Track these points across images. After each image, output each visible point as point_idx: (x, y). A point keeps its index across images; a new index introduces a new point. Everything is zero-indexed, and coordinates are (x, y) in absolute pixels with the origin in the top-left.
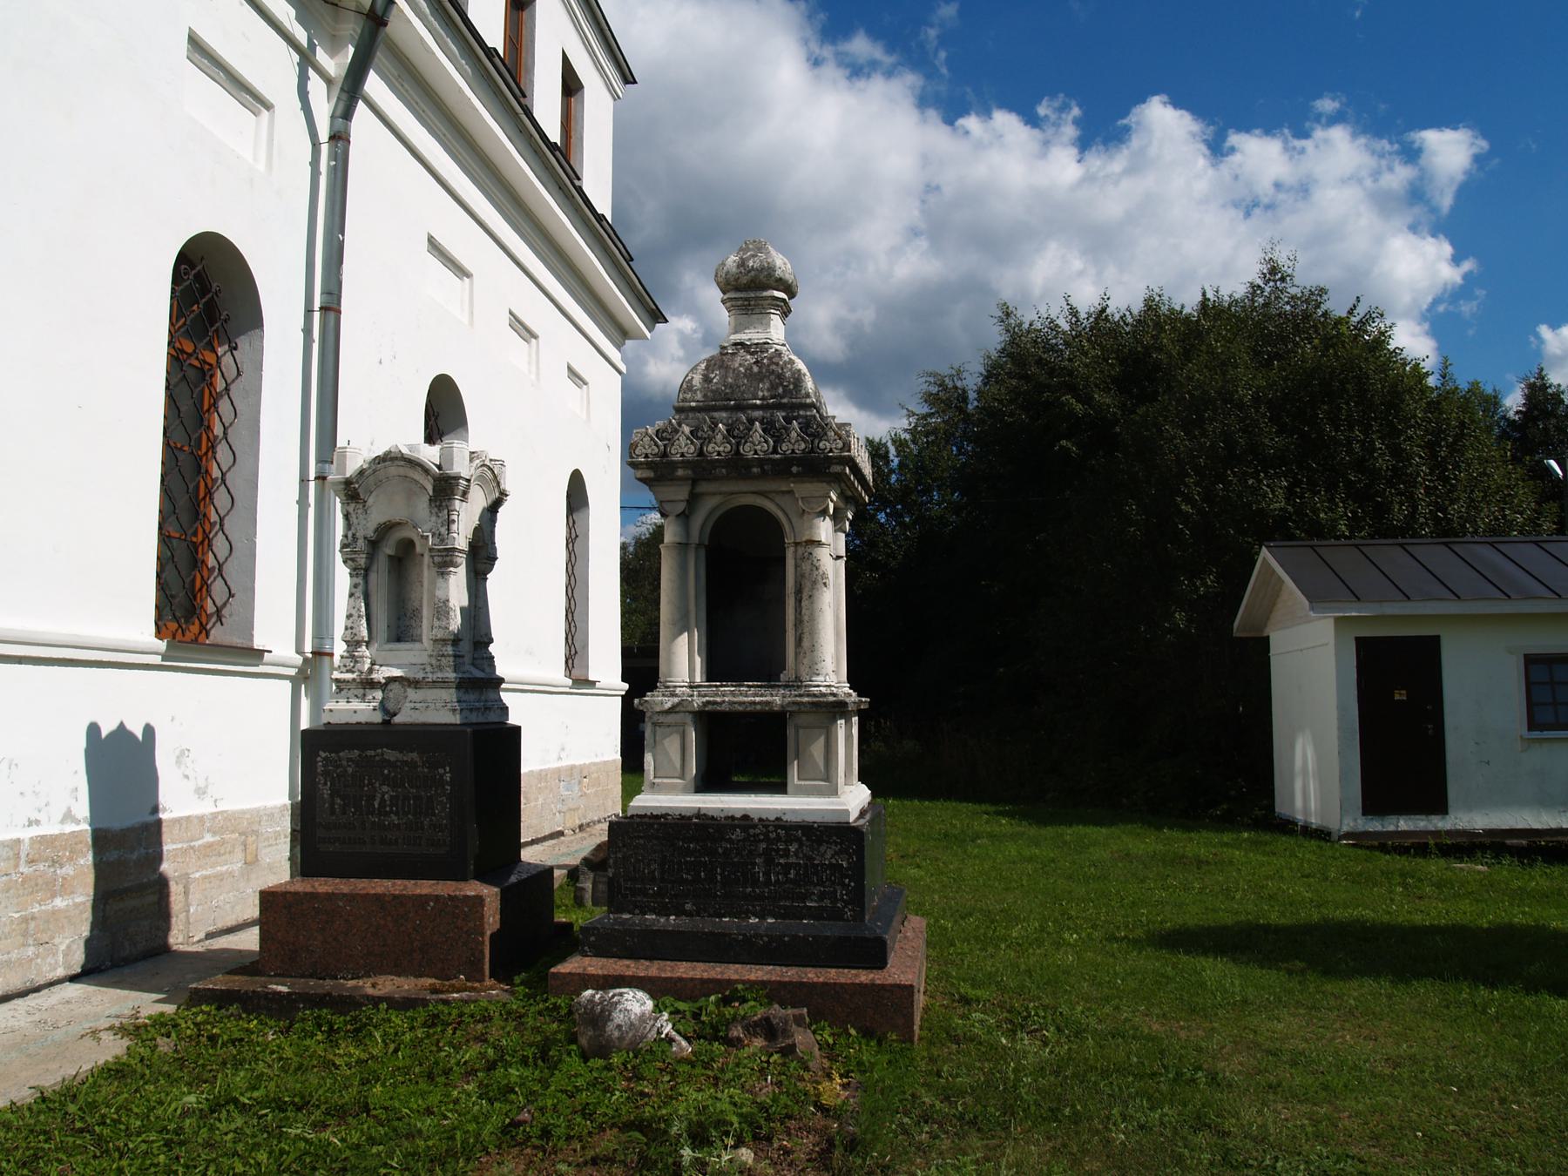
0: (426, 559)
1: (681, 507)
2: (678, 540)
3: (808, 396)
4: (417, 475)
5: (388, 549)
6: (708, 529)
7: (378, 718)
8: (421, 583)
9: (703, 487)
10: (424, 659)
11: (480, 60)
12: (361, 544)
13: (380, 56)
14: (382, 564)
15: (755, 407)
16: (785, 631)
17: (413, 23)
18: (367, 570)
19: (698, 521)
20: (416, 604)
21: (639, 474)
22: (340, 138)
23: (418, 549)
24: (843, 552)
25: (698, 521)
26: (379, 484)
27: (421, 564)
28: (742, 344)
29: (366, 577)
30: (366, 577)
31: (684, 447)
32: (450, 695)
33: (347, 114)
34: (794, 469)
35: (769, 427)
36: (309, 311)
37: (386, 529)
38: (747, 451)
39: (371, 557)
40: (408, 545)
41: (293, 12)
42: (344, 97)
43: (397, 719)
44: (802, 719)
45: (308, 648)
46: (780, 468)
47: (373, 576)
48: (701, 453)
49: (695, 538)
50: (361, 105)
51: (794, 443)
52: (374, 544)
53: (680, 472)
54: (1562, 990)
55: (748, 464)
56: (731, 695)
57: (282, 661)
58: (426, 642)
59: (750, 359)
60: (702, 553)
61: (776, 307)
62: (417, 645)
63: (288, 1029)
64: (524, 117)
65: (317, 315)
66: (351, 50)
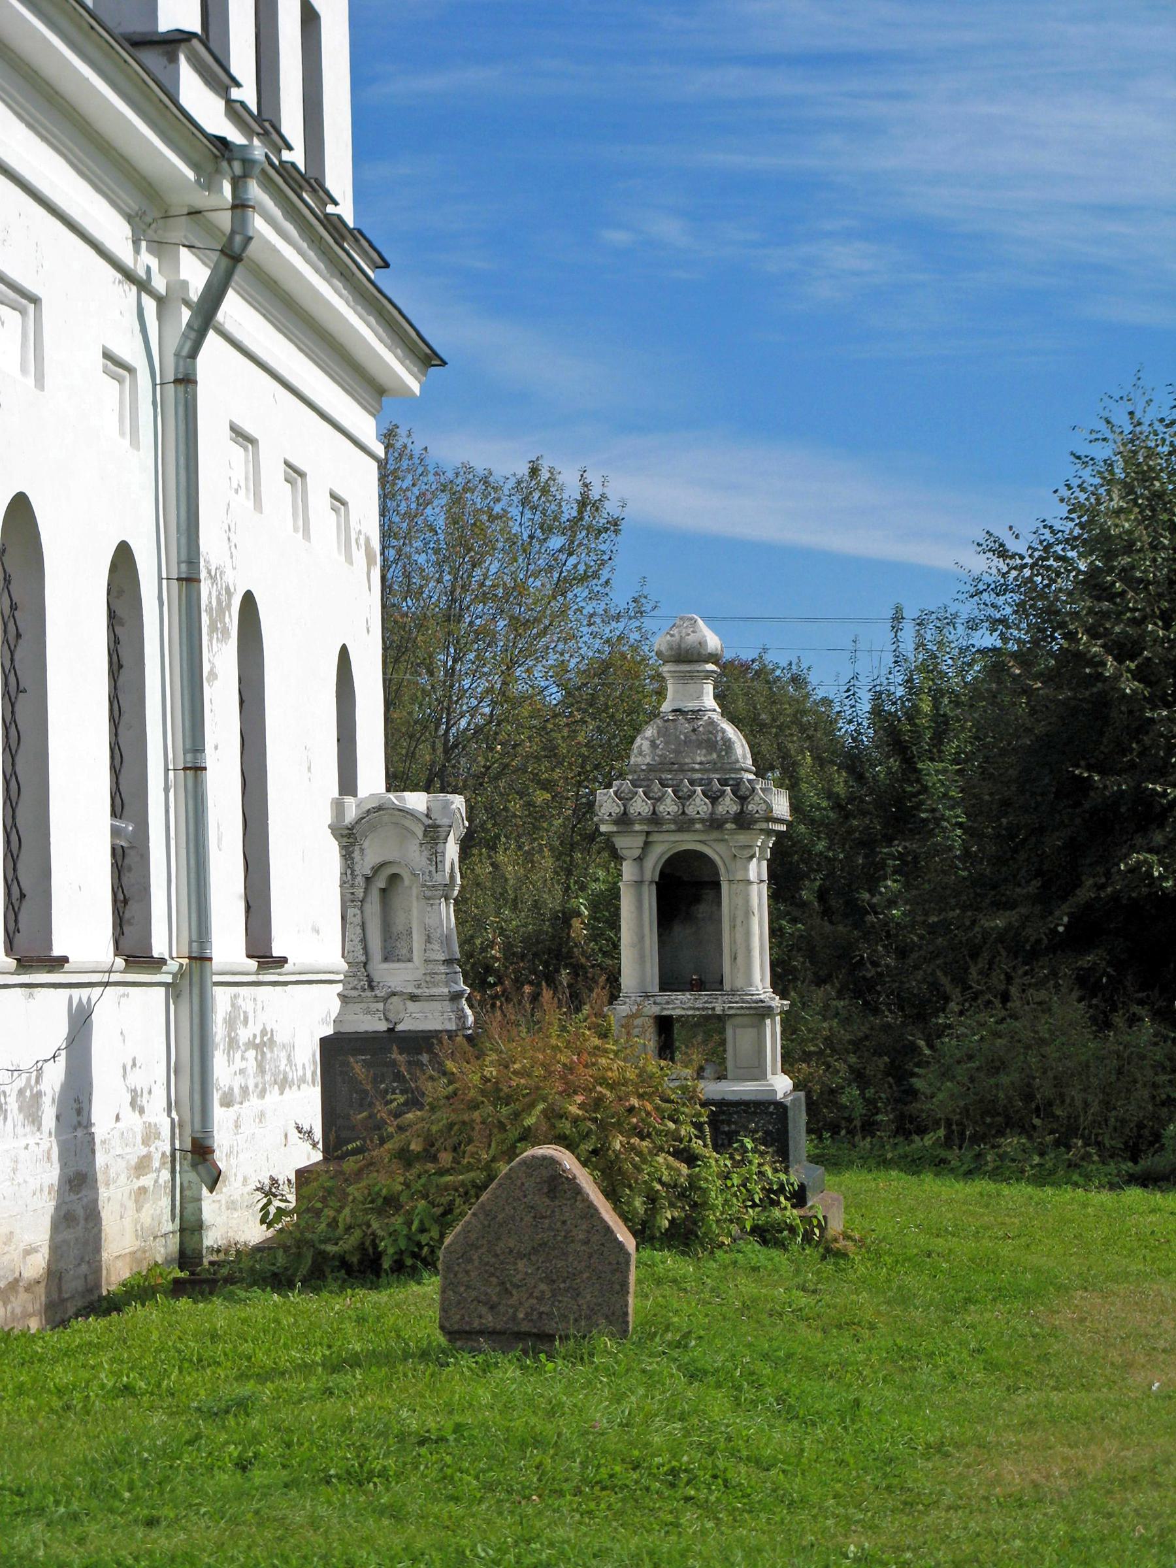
0: (415, 891)
1: (637, 853)
2: (635, 878)
3: (738, 761)
4: (408, 823)
5: (381, 883)
7: (383, 1026)
11: (281, 191)
12: (360, 880)
14: (375, 895)
15: (694, 770)
16: (137, 129)
20: (400, 928)
23: (407, 882)
24: (765, 877)
26: (373, 828)
34: (729, 826)
37: (377, 869)
38: (691, 811)
41: (125, 229)
43: (399, 1028)
44: (738, 1020)
46: (715, 824)
47: (368, 907)
48: (654, 813)
49: (648, 876)
50: (211, 334)
53: (637, 827)
54: (1138, 1158)
55: (692, 821)
56: (681, 1004)
57: (227, 968)
59: (687, 727)
62: (409, 965)
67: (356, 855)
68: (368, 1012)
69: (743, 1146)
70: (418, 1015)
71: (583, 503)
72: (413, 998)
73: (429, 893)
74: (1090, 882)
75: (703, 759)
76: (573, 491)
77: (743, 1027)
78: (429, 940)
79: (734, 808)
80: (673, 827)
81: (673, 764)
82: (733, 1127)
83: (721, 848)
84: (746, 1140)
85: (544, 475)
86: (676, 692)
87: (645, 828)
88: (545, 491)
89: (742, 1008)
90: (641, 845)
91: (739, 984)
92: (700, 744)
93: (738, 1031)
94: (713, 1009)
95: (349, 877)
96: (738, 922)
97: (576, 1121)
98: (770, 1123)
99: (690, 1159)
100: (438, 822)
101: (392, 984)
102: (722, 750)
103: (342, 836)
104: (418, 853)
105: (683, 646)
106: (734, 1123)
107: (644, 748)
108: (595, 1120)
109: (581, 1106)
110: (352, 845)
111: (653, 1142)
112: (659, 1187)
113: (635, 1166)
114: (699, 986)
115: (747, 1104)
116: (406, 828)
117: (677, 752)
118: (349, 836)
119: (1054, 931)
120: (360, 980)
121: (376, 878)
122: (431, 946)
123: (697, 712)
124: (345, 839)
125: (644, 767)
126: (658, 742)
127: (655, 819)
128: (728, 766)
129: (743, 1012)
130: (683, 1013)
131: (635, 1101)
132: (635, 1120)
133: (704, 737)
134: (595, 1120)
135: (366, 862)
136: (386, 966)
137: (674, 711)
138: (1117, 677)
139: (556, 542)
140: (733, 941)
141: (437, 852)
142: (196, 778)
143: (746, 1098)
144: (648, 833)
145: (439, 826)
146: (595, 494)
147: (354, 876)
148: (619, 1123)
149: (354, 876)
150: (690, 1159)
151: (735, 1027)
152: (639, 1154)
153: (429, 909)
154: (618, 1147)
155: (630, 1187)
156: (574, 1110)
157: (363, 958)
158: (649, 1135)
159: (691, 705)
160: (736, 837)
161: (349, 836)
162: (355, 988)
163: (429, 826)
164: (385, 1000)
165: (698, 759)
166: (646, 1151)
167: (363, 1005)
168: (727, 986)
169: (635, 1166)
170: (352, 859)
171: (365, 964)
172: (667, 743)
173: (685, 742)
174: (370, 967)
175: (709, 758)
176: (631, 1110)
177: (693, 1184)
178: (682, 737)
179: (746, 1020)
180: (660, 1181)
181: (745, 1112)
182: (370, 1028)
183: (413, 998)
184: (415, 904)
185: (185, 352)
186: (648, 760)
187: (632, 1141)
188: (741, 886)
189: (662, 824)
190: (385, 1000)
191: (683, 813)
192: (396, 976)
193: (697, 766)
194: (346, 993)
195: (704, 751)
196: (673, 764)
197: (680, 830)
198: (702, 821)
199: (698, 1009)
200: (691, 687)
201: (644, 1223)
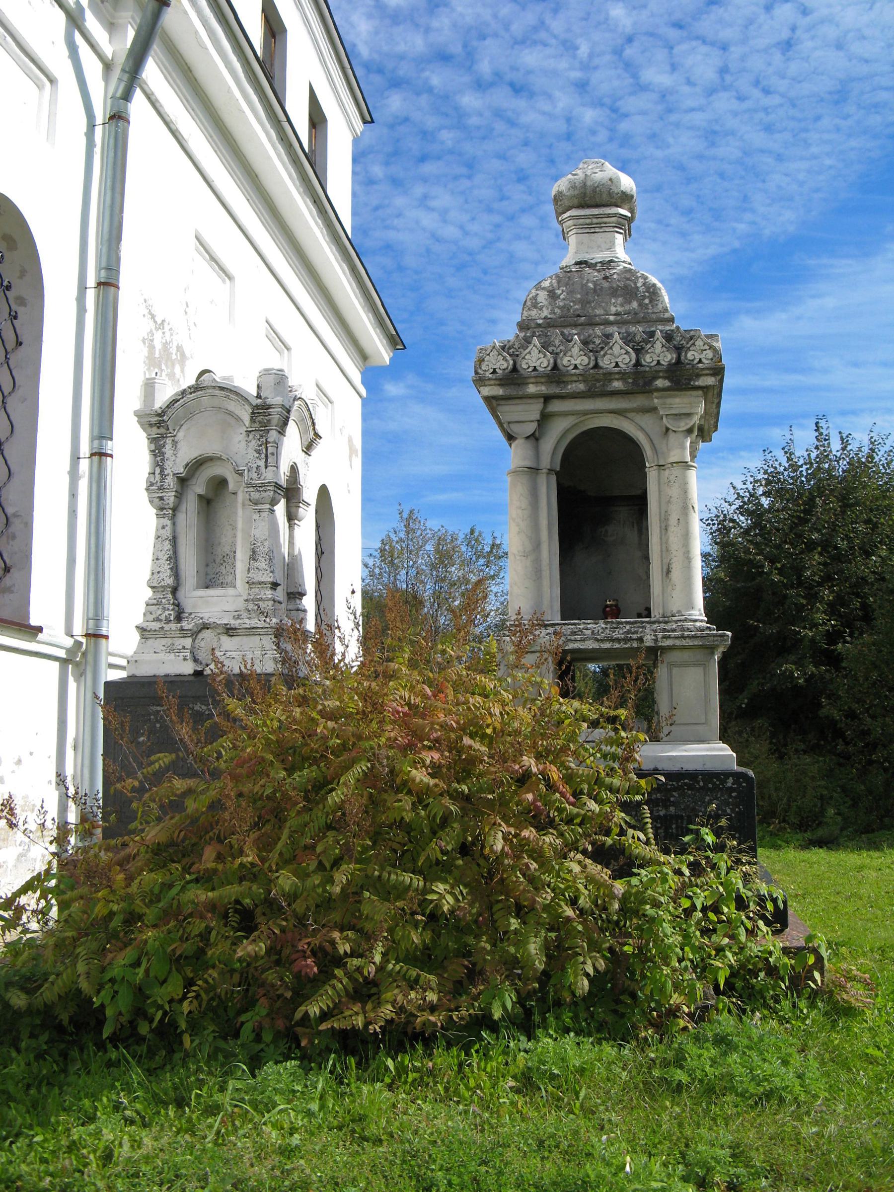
0: (240, 497)
1: (531, 428)
3: (666, 310)
4: (233, 406)
5: (199, 487)
6: (571, 437)
7: (188, 668)
8: (234, 528)
9: (556, 406)
10: (240, 604)
12: (170, 481)
13: (156, 48)
14: (191, 505)
17: (189, 17)
18: (175, 509)
19: (548, 444)
20: (227, 549)
21: (486, 391)
22: (120, 118)
23: (231, 486)
25: (548, 444)
26: (189, 415)
27: (236, 501)
28: (586, 262)
29: (173, 517)
30: (173, 517)
31: (535, 359)
32: (268, 642)
33: (127, 96)
34: (660, 383)
35: (628, 339)
36: (82, 288)
37: (198, 464)
38: (606, 363)
39: (179, 496)
40: (220, 484)
42: (126, 77)
45: (79, 629)
46: (640, 381)
47: (181, 517)
51: (659, 354)
52: (183, 481)
53: (532, 389)
55: (609, 376)
56: (591, 634)
58: (240, 582)
59: (596, 275)
60: (554, 479)
61: (619, 226)
62: (231, 591)
63: (444, 557)
64: (111, 309)
65: (91, 295)
66: (131, 33)
67: (168, 450)
68: (171, 650)
69: (699, 838)
70: (233, 654)
71: (493, 546)
72: (230, 631)
73: (256, 496)
74: (757, 682)
75: (620, 309)
76: (488, 541)
77: (685, 665)
78: (254, 556)
79: (668, 358)
80: (581, 387)
81: (579, 316)
82: (672, 809)
83: (646, 421)
84: (704, 831)
85: (476, 534)
86: (580, 243)
87: (543, 389)
88: (476, 540)
89: (683, 637)
90: (538, 417)
91: (675, 605)
92: (614, 292)
93: (675, 671)
94: (640, 640)
95: (158, 477)
96: (673, 521)
97: (421, 796)
98: (728, 804)
99: (620, 862)
100: (269, 401)
101: (206, 616)
102: (644, 297)
103: (151, 425)
104: (244, 443)
105: (589, 183)
106: (674, 804)
107: (539, 299)
108: (456, 796)
109: (435, 771)
110: (163, 437)
111: (561, 835)
112: (569, 912)
113: (531, 880)
114: (612, 612)
115: (693, 776)
116: (230, 414)
117: (584, 303)
118: (159, 425)
119: (740, 707)
120: (164, 609)
121: (193, 481)
122: (256, 564)
123: (608, 264)
124: (155, 430)
125: (540, 322)
126: (559, 292)
127: (556, 375)
128: (654, 316)
129: (684, 642)
130: (596, 645)
131: (529, 761)
132: (530, 797)
133: (621, 284)
134: (456, 796)
135: (178, 461)
136: (202, 592)
137: (577, 263)
138: (769, 573)
139: (482, 561)
140: (666, 550)
141: (267, 442)
142: (100, 462)
143: (690, 767)
144: (547, 399)
145: (270, 407)
146: (498, 542)
147: (163, 476)
148: (502, 802)
149: (163, 476)
150: (620, 862)
151: (671, 665)
152: (537, 854)
153: (256, 516)
154: (499, 845)
155: (520, 911)
156: (420, 776)
157: (170, 581)
158: (551, 823)
159: (599, 256)
160: (669, 401)
161: (159, 425)
162: (157, 620)
163: (257, 406)
164: (194, 634)
165: (613, 309)
166: (549, 853)
167: (168, 641)
168: (656, 613)
169: (531, 880)
170: (163, 454)
171: (175, 590)
172: (571, 292)
173: (595, 290)
174: (181, 594)
175: (627, 307)
176: (524, 779)
177: (631, 906)
178: (591, 285)
179: (686, 656)
180: (573, 902)
181: (690, 787)
182: (162, 670)
183: (230, 631)
184: (240, 512)
185: (119, 94)
186: (545, 313)
187: (525, 833)
188: (677, 471)
189: (566, 383)
190: (194, 634)
191: (596, 366)
192: (214, 605)
193: (612, 318)
194: (144, 625)
195: (620, 300)
196: (579, 316)
197: (589, 394)
198: (623, 376)
199: (618, 640)
200: (599, 238)
201: (545, 977)
